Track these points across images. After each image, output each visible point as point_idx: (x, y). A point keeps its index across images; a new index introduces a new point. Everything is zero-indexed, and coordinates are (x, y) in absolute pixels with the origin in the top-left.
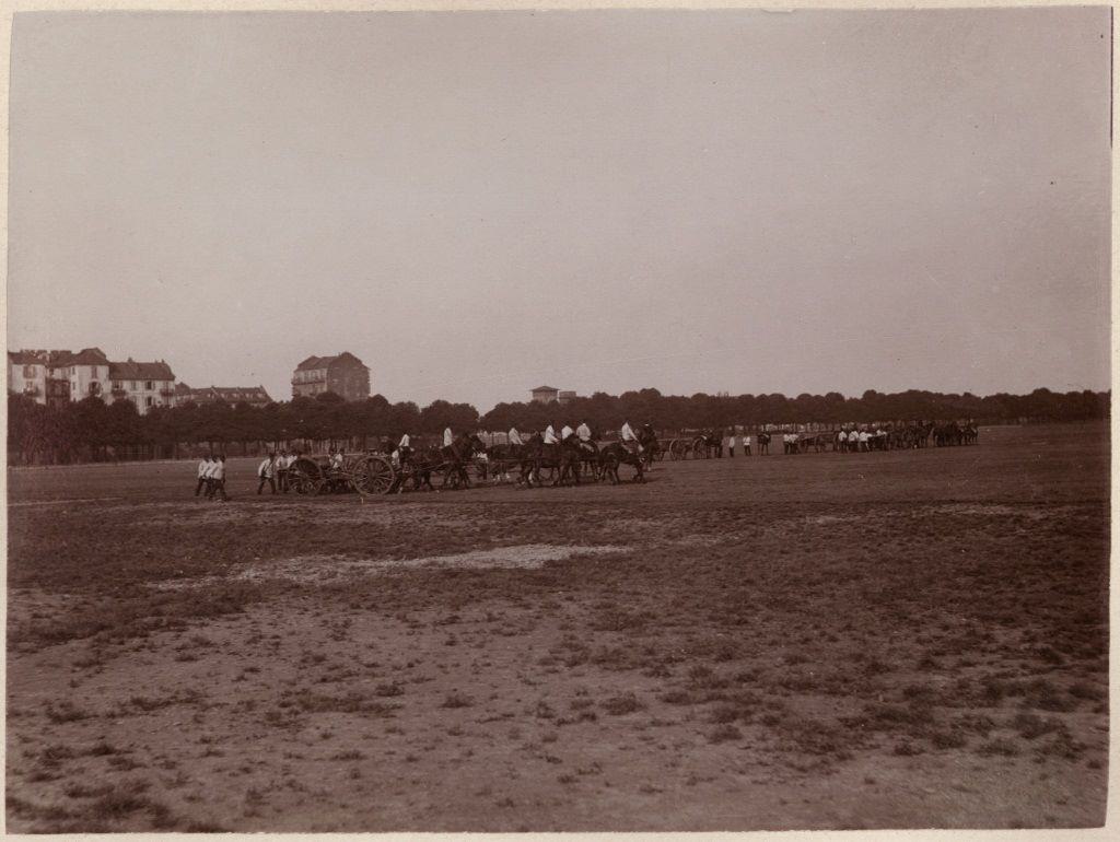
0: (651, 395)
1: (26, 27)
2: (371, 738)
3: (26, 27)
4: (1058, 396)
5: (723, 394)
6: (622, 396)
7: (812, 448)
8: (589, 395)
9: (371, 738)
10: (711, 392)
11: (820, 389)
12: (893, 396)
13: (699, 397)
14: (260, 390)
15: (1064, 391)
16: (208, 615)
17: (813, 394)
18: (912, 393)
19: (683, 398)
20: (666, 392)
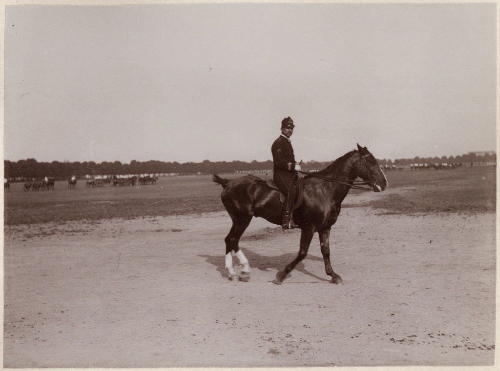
0: (32, 162)
1: (494, 5)
2: (412, 341)
3: (494, 5)
4: (213, 164)
5: (66, 161)
6: (18, 162)
7: (91, 186)
8: (129, 163)
9: (412, 341)
10: (61, 160)
11: (112, 160)
12: (144, 163)
13: (55, 163)
14: (312, 161)
15: (215, 161)
16: (26, 223)
17: (108, 162)
18: (152, 162)
19: (47, 164)
20: (39, 160)
